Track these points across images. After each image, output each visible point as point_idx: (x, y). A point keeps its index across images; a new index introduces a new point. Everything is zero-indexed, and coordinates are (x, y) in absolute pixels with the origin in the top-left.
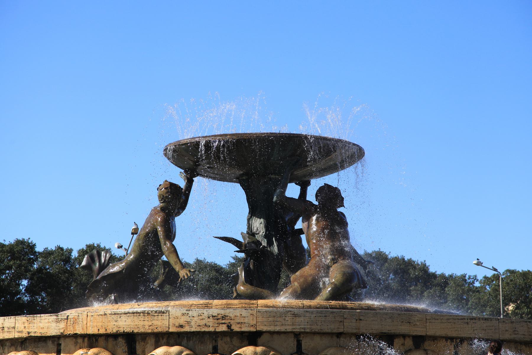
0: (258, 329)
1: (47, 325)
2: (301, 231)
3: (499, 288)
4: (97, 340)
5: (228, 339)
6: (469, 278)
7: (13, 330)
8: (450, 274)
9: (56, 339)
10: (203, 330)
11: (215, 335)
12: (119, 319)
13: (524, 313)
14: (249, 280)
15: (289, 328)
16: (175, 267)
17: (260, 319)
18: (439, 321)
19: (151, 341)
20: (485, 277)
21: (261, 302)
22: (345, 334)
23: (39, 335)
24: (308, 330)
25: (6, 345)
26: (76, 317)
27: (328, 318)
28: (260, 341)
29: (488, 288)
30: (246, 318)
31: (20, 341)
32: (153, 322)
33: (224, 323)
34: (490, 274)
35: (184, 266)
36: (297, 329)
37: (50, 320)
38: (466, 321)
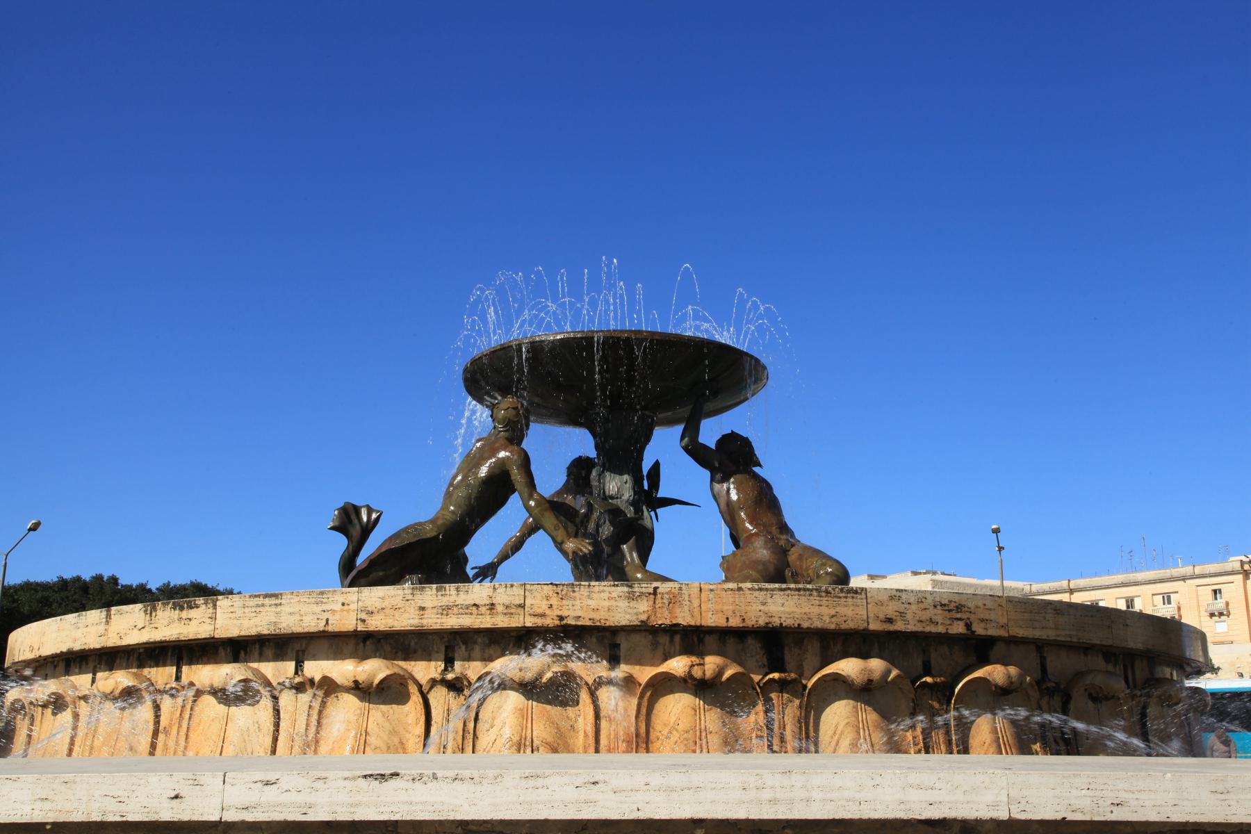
0: (1012, 633)
1: (607, 604)
4: (701, 641)
7: (520, 611)
9: (607, 634)
10: (928, 629)
12: (769, 600)
19: (813, 648)
23: (589, 623)
25: (475, 643)
26: (677, 591)
31: (514, 634)
32: (838, 609)
37: (614, 595)
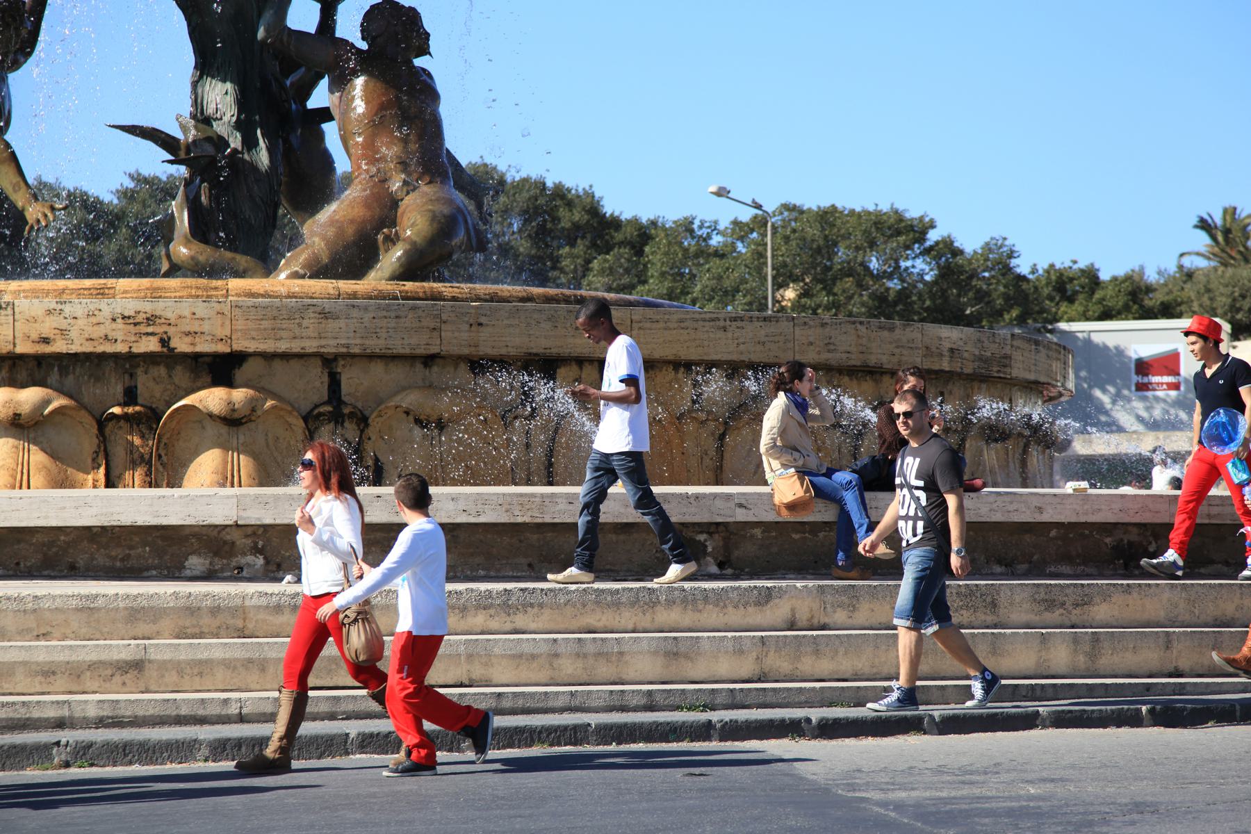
0: (236, 347)
2: (325, 114)
3: (766, 250)
5: (162, 371)
6: (701, 227)
8: (652, 218)
10: (100, 349)
11: (129, 362)
13: (819, 306)
14: (201, 230)
15: (311, 346)
16: (13, 197)
17: (240, 325)
18: (661, 325)
20: (736, 223)
21: (235, 284)
22: (443, 357)
24: (356, 350)
27: (403, 320)
28: (239, 375)
29: (740, 247)
30: (206, 322)
33: (152, 334)
34: (746, 215)
35: (38, 192)
36: (330, 347)
38: (722, 323)
